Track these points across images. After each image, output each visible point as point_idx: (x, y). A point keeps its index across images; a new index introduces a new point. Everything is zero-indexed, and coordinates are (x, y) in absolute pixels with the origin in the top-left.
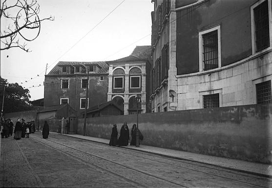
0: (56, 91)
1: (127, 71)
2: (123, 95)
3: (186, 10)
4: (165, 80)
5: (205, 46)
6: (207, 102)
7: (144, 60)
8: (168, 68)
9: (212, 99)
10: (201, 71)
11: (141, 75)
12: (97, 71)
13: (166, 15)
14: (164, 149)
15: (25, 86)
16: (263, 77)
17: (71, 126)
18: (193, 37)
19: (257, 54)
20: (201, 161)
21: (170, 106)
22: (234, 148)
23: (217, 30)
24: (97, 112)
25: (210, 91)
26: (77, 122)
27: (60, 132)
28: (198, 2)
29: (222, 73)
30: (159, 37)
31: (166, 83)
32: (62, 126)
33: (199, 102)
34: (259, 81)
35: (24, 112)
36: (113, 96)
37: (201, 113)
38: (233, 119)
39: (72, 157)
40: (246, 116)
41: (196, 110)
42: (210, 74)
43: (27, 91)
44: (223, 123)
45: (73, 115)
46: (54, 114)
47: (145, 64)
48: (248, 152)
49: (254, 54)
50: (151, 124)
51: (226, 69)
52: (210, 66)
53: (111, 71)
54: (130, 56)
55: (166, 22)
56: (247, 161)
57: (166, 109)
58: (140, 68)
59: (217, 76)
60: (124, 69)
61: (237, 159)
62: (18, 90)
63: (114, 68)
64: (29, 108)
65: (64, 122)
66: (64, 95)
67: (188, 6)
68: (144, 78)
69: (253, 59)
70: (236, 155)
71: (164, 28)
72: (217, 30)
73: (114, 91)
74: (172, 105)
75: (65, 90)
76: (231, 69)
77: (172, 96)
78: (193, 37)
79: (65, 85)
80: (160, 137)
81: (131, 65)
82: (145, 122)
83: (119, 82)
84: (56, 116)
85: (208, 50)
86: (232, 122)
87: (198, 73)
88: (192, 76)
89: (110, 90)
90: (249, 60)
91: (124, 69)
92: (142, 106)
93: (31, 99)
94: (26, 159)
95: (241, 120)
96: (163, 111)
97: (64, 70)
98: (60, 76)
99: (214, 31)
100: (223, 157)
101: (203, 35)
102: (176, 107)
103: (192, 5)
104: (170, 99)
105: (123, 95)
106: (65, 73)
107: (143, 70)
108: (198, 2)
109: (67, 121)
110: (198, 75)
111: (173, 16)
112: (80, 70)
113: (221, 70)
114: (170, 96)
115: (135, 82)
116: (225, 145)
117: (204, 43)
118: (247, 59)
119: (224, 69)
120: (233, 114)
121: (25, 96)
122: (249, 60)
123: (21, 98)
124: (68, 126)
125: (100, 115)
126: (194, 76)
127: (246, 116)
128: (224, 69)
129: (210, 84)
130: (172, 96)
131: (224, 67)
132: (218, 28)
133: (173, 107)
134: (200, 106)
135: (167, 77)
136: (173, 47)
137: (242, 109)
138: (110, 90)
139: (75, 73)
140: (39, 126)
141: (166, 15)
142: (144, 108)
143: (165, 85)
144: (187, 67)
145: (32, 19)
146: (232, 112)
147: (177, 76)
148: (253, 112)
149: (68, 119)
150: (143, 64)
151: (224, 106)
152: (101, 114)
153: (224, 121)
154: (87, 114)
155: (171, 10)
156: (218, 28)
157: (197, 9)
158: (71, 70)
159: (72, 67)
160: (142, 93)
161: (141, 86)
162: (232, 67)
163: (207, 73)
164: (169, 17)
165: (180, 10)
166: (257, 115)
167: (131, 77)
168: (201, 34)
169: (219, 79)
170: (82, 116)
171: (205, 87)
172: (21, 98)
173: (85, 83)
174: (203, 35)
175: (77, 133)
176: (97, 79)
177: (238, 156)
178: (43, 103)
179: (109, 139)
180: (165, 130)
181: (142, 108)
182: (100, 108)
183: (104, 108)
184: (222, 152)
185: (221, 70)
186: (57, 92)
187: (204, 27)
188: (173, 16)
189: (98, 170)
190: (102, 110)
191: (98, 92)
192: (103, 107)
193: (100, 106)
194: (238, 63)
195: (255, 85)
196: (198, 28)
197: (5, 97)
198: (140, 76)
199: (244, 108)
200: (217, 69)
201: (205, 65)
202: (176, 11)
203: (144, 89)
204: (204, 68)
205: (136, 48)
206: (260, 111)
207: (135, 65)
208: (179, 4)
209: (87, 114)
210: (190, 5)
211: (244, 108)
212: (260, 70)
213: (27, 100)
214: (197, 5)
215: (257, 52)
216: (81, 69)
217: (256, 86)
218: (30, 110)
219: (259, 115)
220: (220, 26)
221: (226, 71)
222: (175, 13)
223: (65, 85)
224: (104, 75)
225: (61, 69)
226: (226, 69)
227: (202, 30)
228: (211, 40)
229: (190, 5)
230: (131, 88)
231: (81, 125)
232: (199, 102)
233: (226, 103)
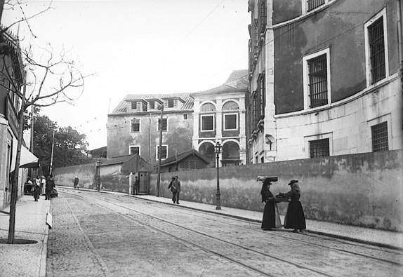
0: (123, 136)
1: (219, 106)
2: (238, 140)
3: (286, 28)
4: (261, 121)
5: (311, 75)
6: (315, 151)
7: (242, 91)
8: (264, 104)
9: (320, 146)
10: (307, 108)
11: (238, 112)
12: (179, 106)
13: (262, 34)
14: (252, 212)
15: (80, 132)
16: (378, 118)
17: (142, 184)
18: (296, 63)
19: (373, 86)
20: (318, 230)
21: (267, 156)
22: (326, 209)
23: (326, 54)
24: (175, 164)
25: (318, 135)
26: (150, 178)
27: (127, 192)
28: (301, 17)
29: (332, 110)
30: (256, 61)
31: (262, 124)
32: (130, 184)
33: (304, 150)
34: (375, 123)
35: (80, 166)
36: (200, 141)
37: (290, 165)
38: (324, 173)
39: (129, 220)
40: (338, 169)
41: (362, 154)
42: (317, 113)
43: (83, 136)
44: (314, 178)
45: (143, 169)
46: (119, 168)
47: (244, 96)
48: (340, 213)
49: (369, 87)
50: (237, 181)
51: (337, 106)
52: (318, 102)
53: (197, 108)
54: (223, 85)
55: (262, 43)
56: (338, 223)
57: (262, 159)
58: (237, 102)
59: (326, 114)
60: (214, 103)
61: (329, 221)
62: (70, 136)
63: (200, 102)
64: (87, 161)
65: (132, 179)
66: (135, 141)
67: (288, 22)
68: (243, 116)
69: (367, 93)
70: (328, 217)
71: (261, 51)
72: (326, 54)
73: (201, 135)
74: (269, 154)
75: (135, 135)
76: (343, 106)
77: (270, 143)
78: (296, 63)
79: (136, 127)
80: (246, 196)
81: (224, 98)
82: (230, 177)
83: (208, 123)
84: (121, 171)
85: (315, 80)
86: (323, 176)
87: (302, 112)
88: (295, 115)
89: (196, 137)
90: (363, 95)
91: (214, 103)
92: (241, 155)
93: (90, 148)
94: (77, 222)
95: (333, 174)
96: (260, 162)
97: (134, 107)
98: (128, 115)
99: (322, 55)
100: (315, 219)
101: (309, 61)
102: (275, 157)
103: (293, 20)
104: (267, 147)
105: (238, 140)
106: (135, 111)
107: (242, 105)
108: (301, 17)
109: (136, 177)
110: (302, 114)
111: (270, 36)
112: (156, 106)
113: (331, 107)
114: (267, 143)
115: (231, 122)
116: (316, 204)
117: (310, 70)
118: (361, 93)
119: (334, 107)
120: (325, 167)
121: (81, 143)
122: (363, 95)
123: (77, 147)
124: (137, 185)
125: (179, 168)
126: (299, 115)
127: (338, 169)
128: (334, 107)
129: (318, 126)
130: (270, 143)
131: (335, 104)
132: (327, 51)
133: (271, 157)
134: (306, 155)
135: (263, 117)
136: (270, 78)
137: (333, 160)
138: (196, 137)
139: (148, 111)
140: (99, 185)
141: (262, 34)
142: (243, 157)
143: (262, 128)
144: (289, 103)
145: (76, 76)
146: (324, 164)
147: (276, 116)
148: (344, 164)
149: (137, 175)
150: (241, 96)
151: (336, 154)
152: (179, 165)
153: (315, 176)
154: (161, 168)
155: (267, 27)
156: (327, 51)
157: (300, 26)
158: (143, 107)
159: (144, 103)
160: (240, 136)
161: (239, 128)
162: (345, 103)
163: (314, 111)
164: (264, 36)
165: (279, 28)
166: (348, 168)
167: (224, 114)
168: (305, 59)
169: (329, 119)
170: (156, 170)
171: (311, 130)
172: (77, 147)
173: (163, 124)
174: (309, 61)
175: (149, 194)
176: (179, 118)
177: (330, 218)
178: (106, 152)
179: (261, 211)
180: (251, 188)
181: (241, 158)
182: (178, 160)
183: (184, 159)
184: (313, 214)
185: (331, 107)
186: (124, 138)
187: (309, 50)
188: (270, 36)
189: (152, 230)
190: (181, 161)
191: (181, 136)
192: (182, 158)
193: (178, 156)
194: (351, 98)
195: (370, 128)
196: (302, 52)
197: (55, 145)
198: (237, 114)
199: (335, 159)
200: (325, 106)
201: (312, 101)
202: (273, 29)
203: (243, 132)
204: (310, 105)
205: (232, 74)
206: (351, 163)
207: (229, 97)
208: (277, 20)
209: (161, 168)
210: (291, 21)
211: (335, 159)
212: (376, 108)
213: (84, 148)
214: (301, 20)
215: (372, 84)
216: (156, 104)
217: (372, 130)
218: (88, 163)
219: (351, 168)
220: (329, 49)
221: (336, 108)
222: (272, 31)
223: (136, 127)
224: (188, 112)
225: (130, 104)
226: (337, 106)
227: (307, 54)
228: (318, 66)
229: (291, 21)
230: (224, 130)
231: (154, 183)
232: (304, 150)
233: (338, 151)
